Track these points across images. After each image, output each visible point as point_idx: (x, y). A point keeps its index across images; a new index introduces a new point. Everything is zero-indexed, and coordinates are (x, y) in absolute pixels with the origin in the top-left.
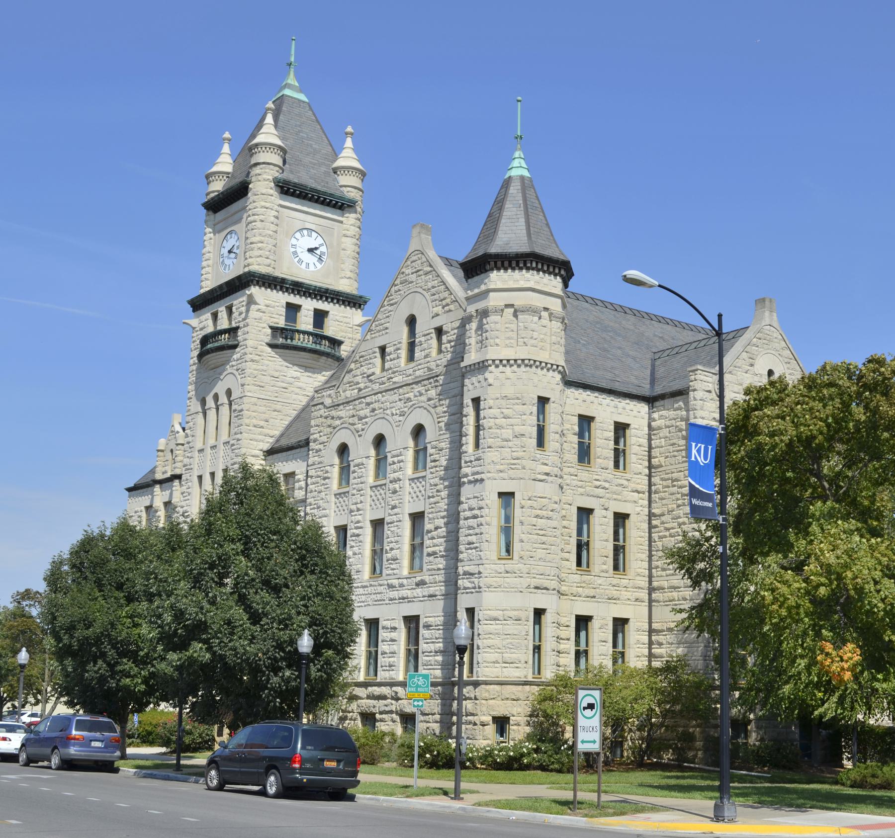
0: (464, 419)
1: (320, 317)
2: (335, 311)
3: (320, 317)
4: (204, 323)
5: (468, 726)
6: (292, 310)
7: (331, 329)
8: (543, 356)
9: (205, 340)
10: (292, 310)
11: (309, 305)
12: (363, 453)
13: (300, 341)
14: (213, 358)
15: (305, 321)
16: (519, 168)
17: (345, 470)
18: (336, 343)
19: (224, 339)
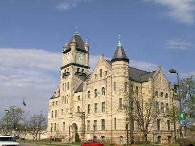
0: (127, 75)
1: (83, 70)
2: (85, 69)
3: (83, 70)
4: (63, 71)
5: (161, 127)
6: (78, 69)
7: (84, 72)
8: (120, 75)
9: (63, 74)
10: (78, 69)
11: (81, 68)
12: (92, 92)
13: (79, 74)
14: (65, 77)
15: (80, 71)
16: (120, 45)
17: (89, 95)
18: (85, 74)
19: (67, 74)
